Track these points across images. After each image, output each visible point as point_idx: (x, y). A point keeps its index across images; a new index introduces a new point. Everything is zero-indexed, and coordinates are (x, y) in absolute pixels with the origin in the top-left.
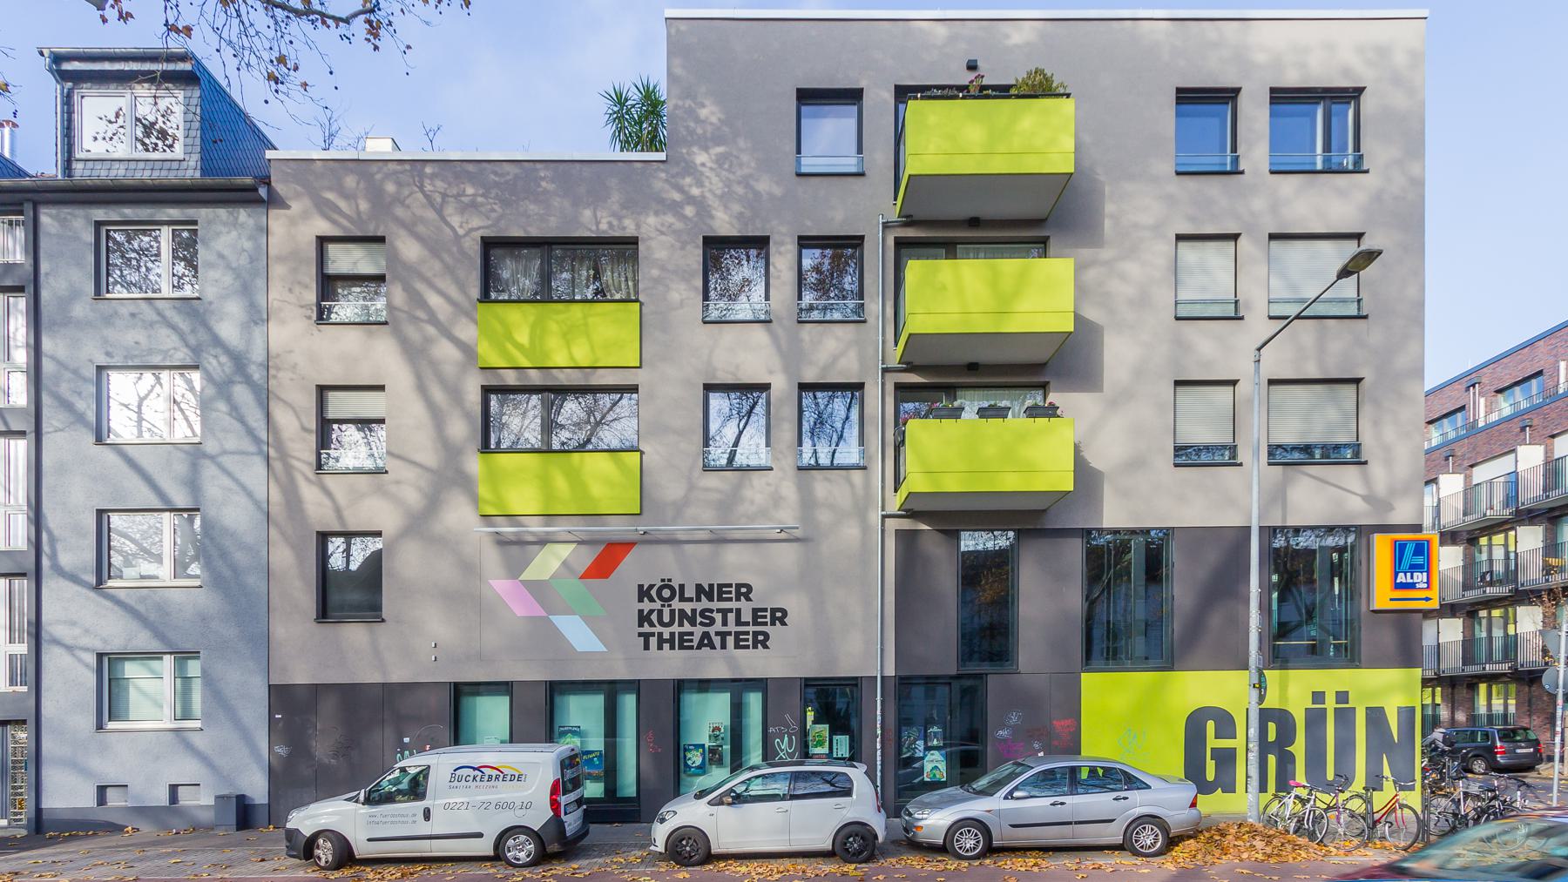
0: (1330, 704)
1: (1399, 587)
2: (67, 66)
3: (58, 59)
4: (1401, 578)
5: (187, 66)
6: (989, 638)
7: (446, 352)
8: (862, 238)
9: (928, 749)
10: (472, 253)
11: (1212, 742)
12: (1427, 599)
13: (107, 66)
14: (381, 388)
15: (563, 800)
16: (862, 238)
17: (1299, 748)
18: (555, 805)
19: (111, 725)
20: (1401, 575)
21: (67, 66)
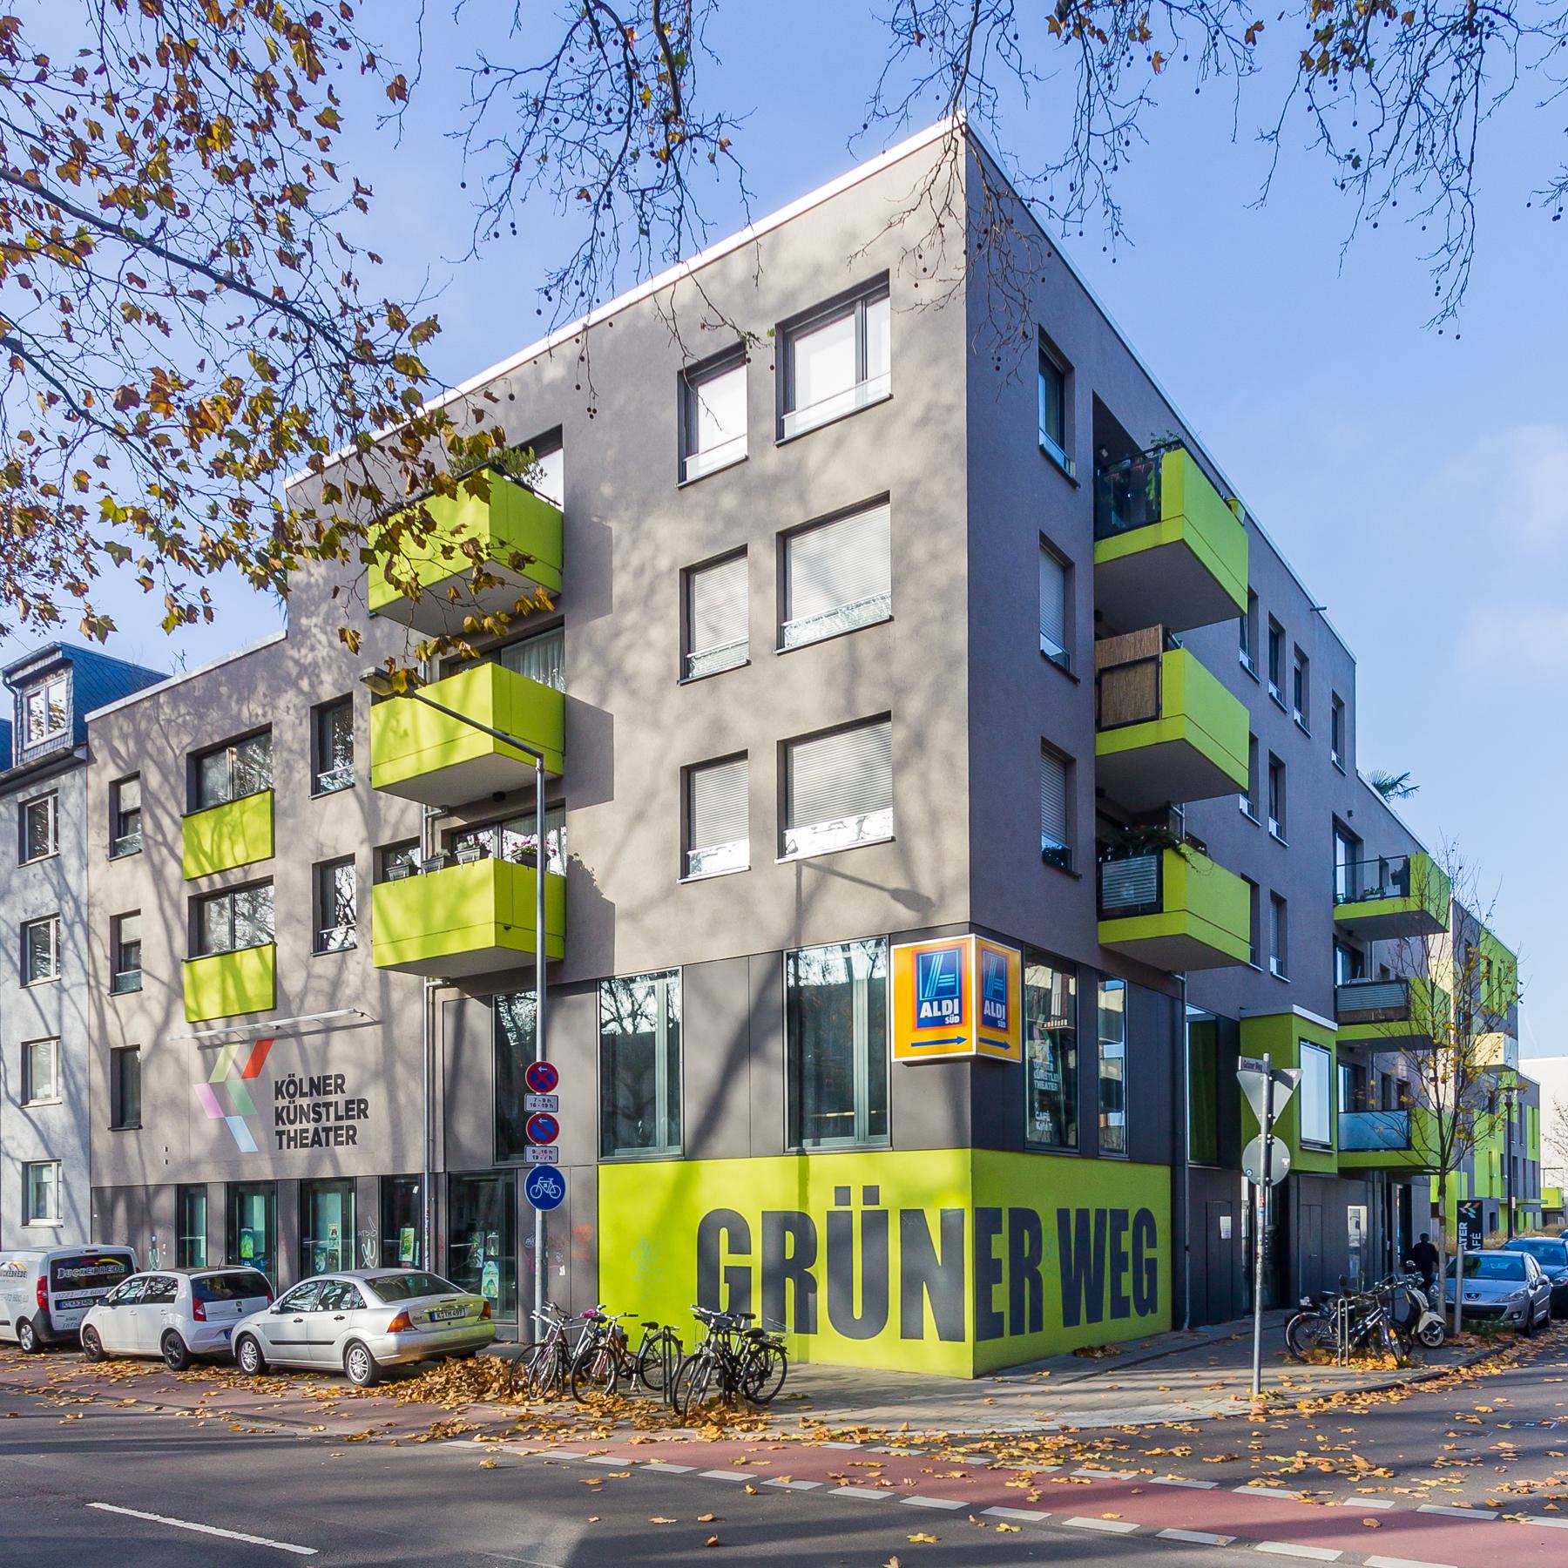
0: (857, 1207)
1: (922, 1023)
2: (16, 677)
3: (8, 673)
4: (926, 1011)
5: (59, 655)
6: (518, 1129)
7: (172, 869)
8: (1059, 1211)
9: (487, 1258)
10: (63, 705)
11: (727, 1259)
12: (960, 1040)
13: (30, 670)
14: (137, 912)
15: (53, 1297)
16: (1059, 1211)
17: (820, 1270)
18: (43, 1302)
19: (33, 1222)
20: (926, 1005)
21: (16, 677)
